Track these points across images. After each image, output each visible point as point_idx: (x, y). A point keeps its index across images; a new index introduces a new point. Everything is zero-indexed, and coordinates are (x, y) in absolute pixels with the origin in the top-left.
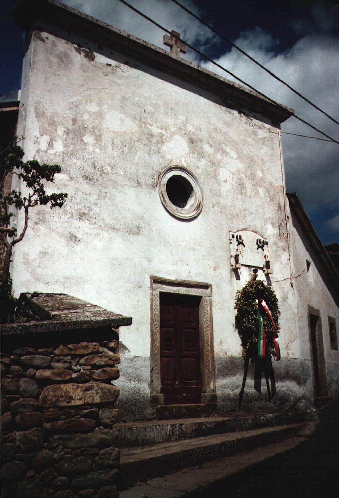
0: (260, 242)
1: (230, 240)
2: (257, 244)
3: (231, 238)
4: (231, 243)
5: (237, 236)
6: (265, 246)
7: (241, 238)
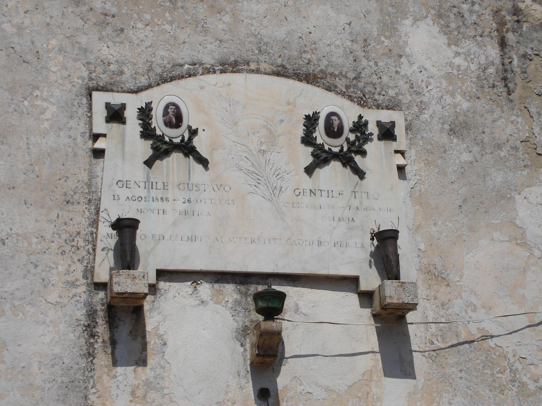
0: (334, 131)
1: (96, 137)
2: (308, 140)
3: (100, 125)
4: (99, 153)
5: (145, 113)
6: (374, 147)
7: (175, 117)
